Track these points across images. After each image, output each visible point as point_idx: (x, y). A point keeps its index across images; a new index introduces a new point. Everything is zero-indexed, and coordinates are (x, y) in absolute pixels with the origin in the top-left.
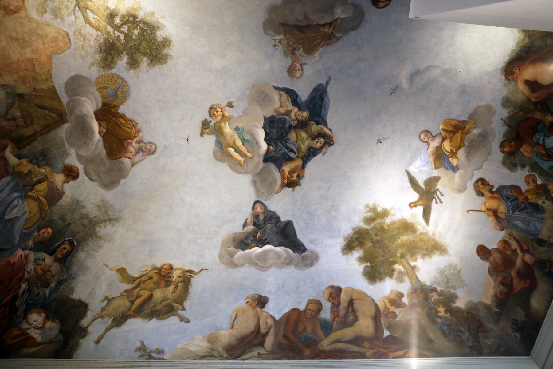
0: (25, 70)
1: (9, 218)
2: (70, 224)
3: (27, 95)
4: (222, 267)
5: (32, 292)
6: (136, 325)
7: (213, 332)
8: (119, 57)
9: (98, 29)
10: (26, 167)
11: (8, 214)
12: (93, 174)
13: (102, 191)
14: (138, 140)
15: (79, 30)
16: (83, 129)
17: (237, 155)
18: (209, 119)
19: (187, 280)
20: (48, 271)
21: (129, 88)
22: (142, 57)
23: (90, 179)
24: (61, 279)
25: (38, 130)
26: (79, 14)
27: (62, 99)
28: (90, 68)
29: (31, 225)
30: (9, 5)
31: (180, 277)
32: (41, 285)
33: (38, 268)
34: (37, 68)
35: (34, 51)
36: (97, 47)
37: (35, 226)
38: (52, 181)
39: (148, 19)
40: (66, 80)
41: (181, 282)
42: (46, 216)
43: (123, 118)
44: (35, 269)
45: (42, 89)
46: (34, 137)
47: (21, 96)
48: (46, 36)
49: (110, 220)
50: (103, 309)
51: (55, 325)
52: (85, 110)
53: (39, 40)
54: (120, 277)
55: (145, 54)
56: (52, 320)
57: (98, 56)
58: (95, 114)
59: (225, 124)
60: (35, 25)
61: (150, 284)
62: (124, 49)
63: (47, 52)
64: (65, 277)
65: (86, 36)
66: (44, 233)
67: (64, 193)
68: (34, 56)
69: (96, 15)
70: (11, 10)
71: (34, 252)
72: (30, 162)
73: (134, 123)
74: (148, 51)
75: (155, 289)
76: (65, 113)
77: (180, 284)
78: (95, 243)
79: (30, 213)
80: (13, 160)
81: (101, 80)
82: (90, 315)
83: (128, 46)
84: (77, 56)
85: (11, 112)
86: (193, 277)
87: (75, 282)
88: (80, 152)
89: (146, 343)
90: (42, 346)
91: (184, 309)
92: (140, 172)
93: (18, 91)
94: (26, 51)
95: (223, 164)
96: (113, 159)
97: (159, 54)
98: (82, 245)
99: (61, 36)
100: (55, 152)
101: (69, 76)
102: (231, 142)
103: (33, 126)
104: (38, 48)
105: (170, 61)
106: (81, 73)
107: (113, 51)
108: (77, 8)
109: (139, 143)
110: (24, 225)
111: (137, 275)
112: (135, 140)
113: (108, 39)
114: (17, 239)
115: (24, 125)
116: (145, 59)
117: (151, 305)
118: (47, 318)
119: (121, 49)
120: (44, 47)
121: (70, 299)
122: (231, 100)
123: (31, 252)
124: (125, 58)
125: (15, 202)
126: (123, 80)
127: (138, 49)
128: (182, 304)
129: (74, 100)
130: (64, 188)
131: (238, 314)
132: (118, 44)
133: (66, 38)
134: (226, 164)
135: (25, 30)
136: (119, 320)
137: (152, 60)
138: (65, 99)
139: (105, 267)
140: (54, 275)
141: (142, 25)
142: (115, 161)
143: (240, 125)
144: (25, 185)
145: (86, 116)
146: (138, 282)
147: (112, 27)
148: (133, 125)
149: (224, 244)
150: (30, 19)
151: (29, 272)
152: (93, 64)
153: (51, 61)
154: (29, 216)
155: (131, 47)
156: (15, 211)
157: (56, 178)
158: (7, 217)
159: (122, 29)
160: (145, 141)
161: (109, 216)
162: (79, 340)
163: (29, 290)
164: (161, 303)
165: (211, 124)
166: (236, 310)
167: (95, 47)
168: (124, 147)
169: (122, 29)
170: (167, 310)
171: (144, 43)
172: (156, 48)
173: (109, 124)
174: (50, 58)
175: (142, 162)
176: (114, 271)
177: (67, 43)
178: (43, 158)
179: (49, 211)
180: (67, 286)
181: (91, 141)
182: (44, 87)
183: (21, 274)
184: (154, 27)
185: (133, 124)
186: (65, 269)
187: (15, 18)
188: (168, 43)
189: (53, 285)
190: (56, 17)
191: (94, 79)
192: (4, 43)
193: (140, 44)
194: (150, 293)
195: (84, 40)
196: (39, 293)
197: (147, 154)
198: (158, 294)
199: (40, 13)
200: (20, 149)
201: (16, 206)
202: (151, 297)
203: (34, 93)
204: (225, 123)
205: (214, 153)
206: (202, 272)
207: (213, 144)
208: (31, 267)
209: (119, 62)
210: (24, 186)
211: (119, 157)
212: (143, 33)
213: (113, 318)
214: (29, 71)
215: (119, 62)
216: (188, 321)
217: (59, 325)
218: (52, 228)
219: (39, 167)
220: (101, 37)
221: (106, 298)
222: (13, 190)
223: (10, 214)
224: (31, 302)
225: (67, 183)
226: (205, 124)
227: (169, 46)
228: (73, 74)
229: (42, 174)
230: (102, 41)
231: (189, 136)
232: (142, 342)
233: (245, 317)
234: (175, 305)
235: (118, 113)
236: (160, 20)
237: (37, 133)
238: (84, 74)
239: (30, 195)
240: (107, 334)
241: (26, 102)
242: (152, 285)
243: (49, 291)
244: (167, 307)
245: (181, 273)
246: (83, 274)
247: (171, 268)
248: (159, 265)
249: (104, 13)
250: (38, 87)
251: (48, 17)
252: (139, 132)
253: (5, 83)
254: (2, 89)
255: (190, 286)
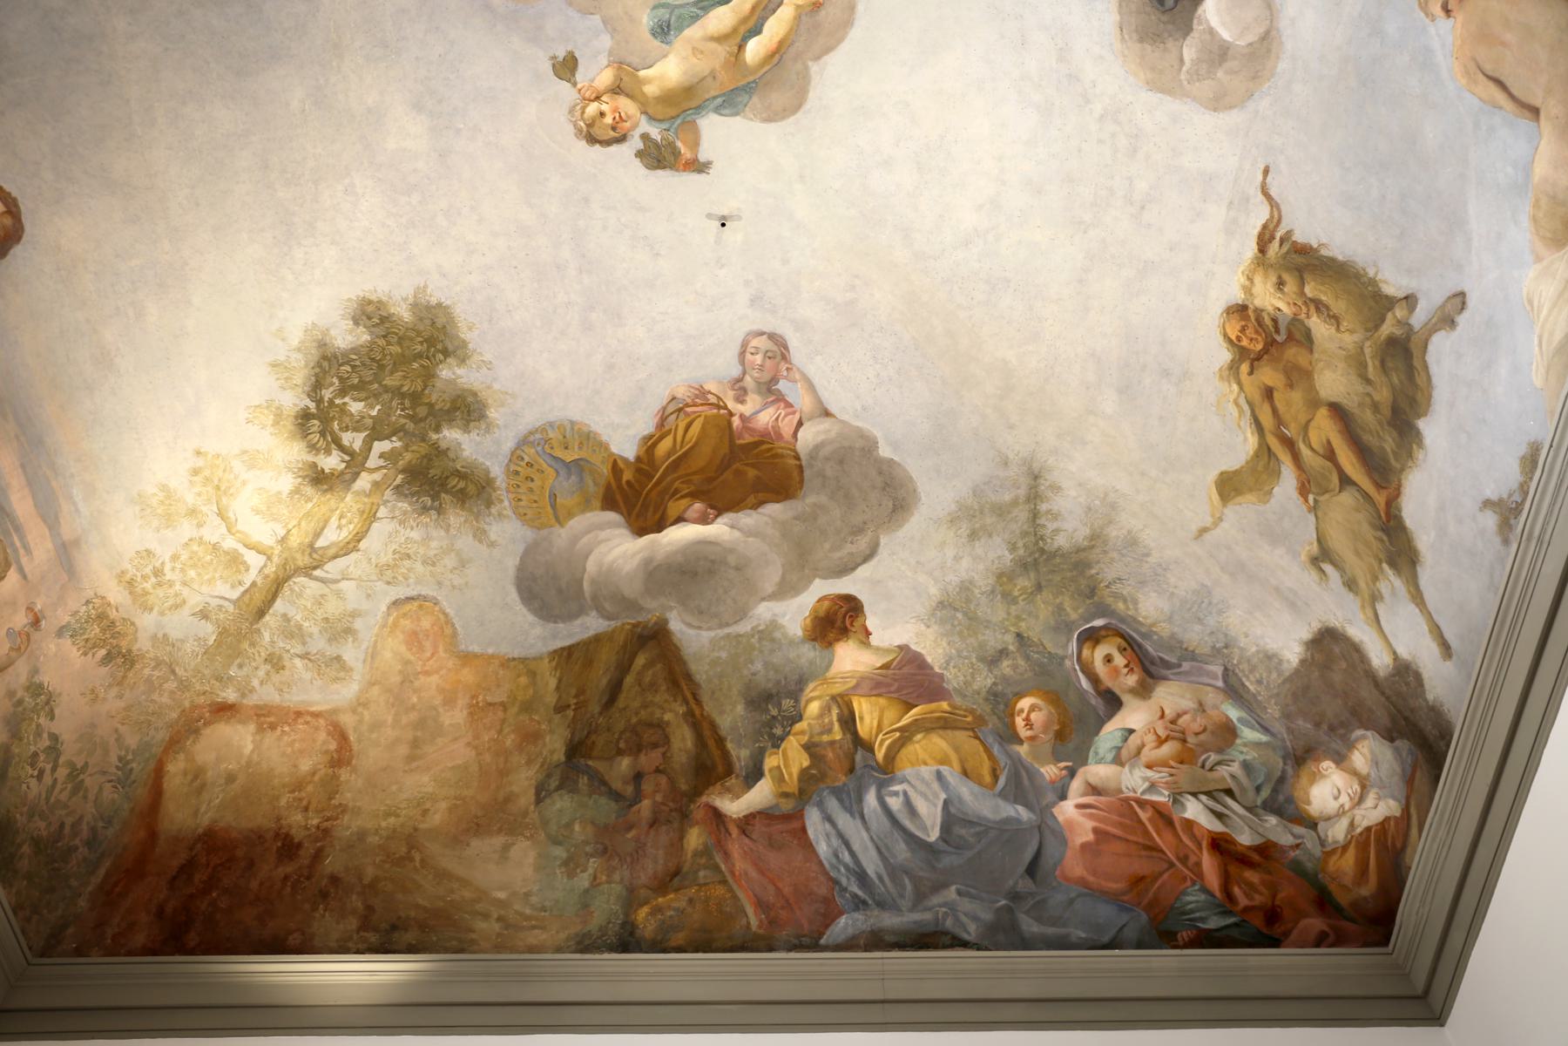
0: (500, 732)
1: (937, 829)
2: (1019, 635)
3: (573, 734)
4: (1263, 103)
5: (1231, 784)
6: (1424, 497)
7: (1526, 209)
8: (451, 455)
9: (370, 517)
10: (791, 758)
11: (925, 829)
12: (849, 548)
13: (915, 524)
14: (731, 393)
15: (381, 569)
16: (690, 574)
17: (775, 27)
18: (635, 143)
19: (1299, 259)
20: (1173, 722)
21: (551, 424)
22: (438, 384)
23: (867, 558)
24: (1220, 684)
25: (682, 710)
26: (332, 569)
27: (591, 633)
28: (492, 545)
29: (987, 765)
30: (327, 752)
31: (1280, 284)
32: (1220, 751)
33: (1149, 754)
34: (499, 696)
35: (449, 701)
36: (425, 519)
37: (996, 750)
38: (854, 682)
39: (301, 376)
40: (531, 618)
41: (1302, 283)
42: (972, 712)
43: (655, 444)
44: (1149, 767)
45: (558, 688)
46: (702, 727)
47: (576, 750)
48: (407, 663)
49: (1034, 497)
50: (1351, 585)
51: (1366, 743)
52: (630, 566)
53: (417, 684)
54: (1250, 497)
55: (429, 376)
56: (1351, 746)
57: (455, 517)
58: (641, 532)
59: (648, 81)
60: (376, 690)
61: (1292, 402)
62: (423, 440)
63: (450, 664)
64: (1219, 670)
65: (394, 552)
66: (1029, 723)
67: (904, 648)
68: (462, 701)
69: (326, 522)
70: (339, 751)
71: (1084, 762)
72: (777, 742)
73: (670, 409)
74: (415, 365)
75: (1311, 389)
76: (635, 626)
77: (1309, 290)
78: (1115, 555)
79: (944, 761)
80: (760, 795)
81: (529, 512)
82: (1359, 631)
83: (410, 426)
84: (457, 581)
85: (617, 785)
86: (1289, 233)
87: (1243, 642)
88: (769, 588)
89: (1491, 492)
90: (1413, 811)
91: (1410, 300)
92: (850, 387)
93: (560, 756)
94: (447, 722)
95: (815, 80)
96: (802, 481)
97: (419, 333)
98: (1109, 600)
99: (403, 622)
100: (758, 666)
101: (519, 607)
102: (722, 51)
103: (668, 723)
104: (441, 690)
105: (437, 293)
106: (512, 572)
107: (432, 472)
108: (317, 573)
109: (744, 391)
110: (980, 784)
111: (1251, 442)
112: (731, 405)
113: (397, 487)
114: (1023, 813)
115: (662, 750)
116: (445, 372)
117: (1368, 417)
118: (1340, 759)
119: (423, 449)
120: (437, 672)
121: (1297, 671)
122: (547, 67)
123: (1081, 770)
124: (451, 435)
125: (895, 803)
126: (524, 442)
127: (415, 398)
128: (1390, 303)
129: (595, 597)
130: (885, 644)
131: (1488, 68)
132: (408, 456)
133: (407, 607)
134: (814, 68)
135: (390, 719)
136: (1396, 545)
137: (446, 353)
138: (591, 625)
139: (1207, 536)
140: (1201, 704)
141: (327, 394)
142: (807, 473)
143: (646, 20)
144: (851, 766)
145: (647, 562)
146: (1277, 442)
147: (356, 475)
148: (680, 410)
149: (1164, 83)
150: (360, 704)
151: (1153, 787)
152: (480, 535)
153: (476, 656)
154: (956, 764)
155: (411, 418)
156: (922, 806)
157: (849, 668)
158: (934, 835)
159: (357, 446)
160: (736, 371)
161: (1015, 503)
162: (1426, 700)
163: (1217, 794)
164: (1368, 381)
165: (655, 133)
166: (1467, 73)
167: (427, 525)
168: (757, 444)
169: (357, 446)
170: (1400, 362)
171: (388, 382)
172: (399, 343)
173: (676, 491)
174: (466, 658)
175: (816, 381)
176: (1226, 511)
177: (421, 607)
178: (774, 705)
179: (958, 700)
180: (1253, 669)
181: (732, 551)
182: (553, 683)
183: (1144, 816)
184: (325, 358)
185: (673, 413)
186: (1186, 666)
187: (359, 741)
188: (370, 309)
189: (1234, 713)
190: (349, 631)
191: (529, 534)
192: (426, 779)
193: (398, 392)
194: (1323, 412)
195: (409, 556)
196: (1246, 766)
197: (783, 366)
198: (1333, 382)
199: (342, 674)
200: (729, 771)
201: (908, 803)
202: (1337, 410)
203: (570, 713)
204: (641, 82)
205: (771, 117)
206: (1273, 192)
207: (737, 121)
208: (1134, 780)
209: (466, 454)
210: (852, 770)
211: (793, 462)
212: (354, 387)
213: (1385, 566)
214: (503, 721)
215: (466, 454)
216: (1460, 300)
217: (1369, 733)
218: (1020, 695)
219: (800, 718)
220: (394, 506)
221: (1315, 561)
222: (854, 805)
223: (929, 823)
224: (1265, 793)
225: (868, 634)
226: (658, 157)
227: (380, 304)
228: (513, 595)
229: (826, 710)
230: (405, 505)
231: (709, 216)
232: (1487, 504)
233: (1509, 37)
234: (1387, 329)
235: (638, 459)
236: (295, 343)
237: (690, 714)
238: (512, 563)
239: (886, 756)
240: (1431, 605)
241: (593, 737)
242: (1297, 396)
243: (1252, 728)
244: (1390, 365)
245: (1266, 276)
246: (1220, 612)
247: (1239, 310)
248: (1225, 356)
249: (316, 502)
250: (551, 699)
251: (351, 654)
252: (702, 393)
253: (533, 791)
254: (548, 801)
255: (1324, 252)
